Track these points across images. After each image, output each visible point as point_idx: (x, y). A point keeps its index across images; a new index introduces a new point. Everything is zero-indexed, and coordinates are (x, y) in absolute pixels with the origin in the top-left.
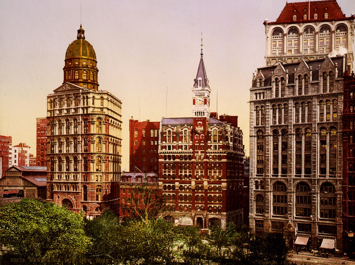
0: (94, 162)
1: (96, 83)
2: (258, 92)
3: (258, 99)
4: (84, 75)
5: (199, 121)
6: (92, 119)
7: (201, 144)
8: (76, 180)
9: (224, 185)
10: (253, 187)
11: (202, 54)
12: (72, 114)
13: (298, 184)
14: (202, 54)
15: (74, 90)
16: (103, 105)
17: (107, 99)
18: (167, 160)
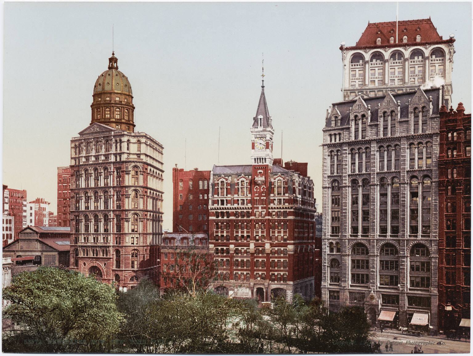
1: (131, 122)
2: (333, 132)
3: (157, 215)
4: (117, 113)
5: (259, 169)
6: (127, 168)
7: (262, 198)
9: (291, 247)
10: (326, 250)
11: (263, 87)
13: (383, 246)
14: (263, 87)
16: (140, 151)
17: (146, 143)
18: (220, 218)
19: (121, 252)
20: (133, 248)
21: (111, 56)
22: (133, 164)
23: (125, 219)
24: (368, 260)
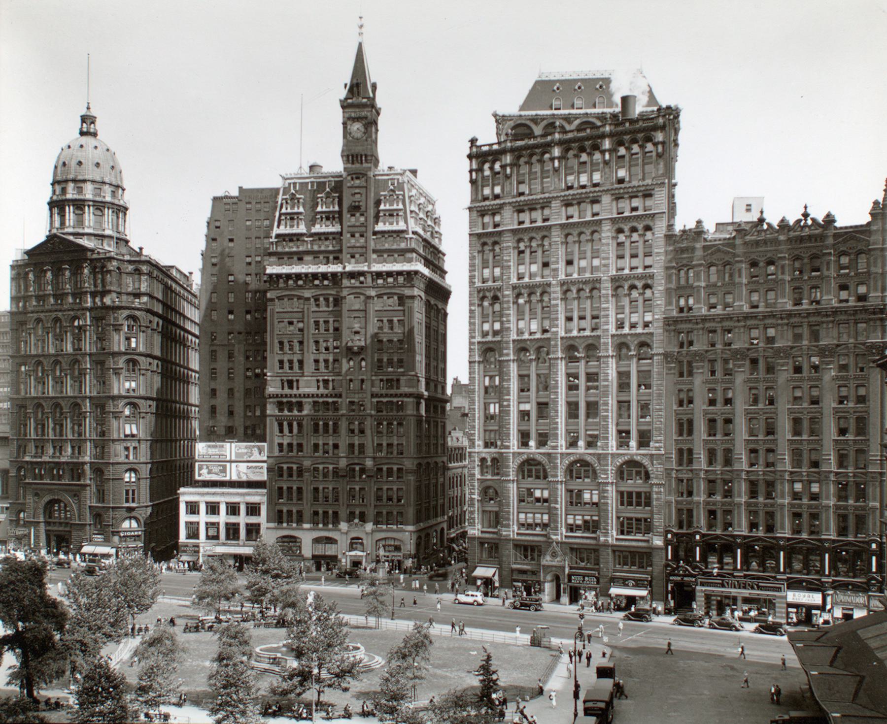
0: (119, 417)
6: (116, 319)
8: (59, 458)
12: (50, 307)
13: (572, 464)
15: (70, 251)
17: (150, 274)
18: (286, 412)
19: (106, 472)
20: (128, 467)
21: (84, 112)
22: (126, 313)
23: (113, 413)
24: (650, 493)
